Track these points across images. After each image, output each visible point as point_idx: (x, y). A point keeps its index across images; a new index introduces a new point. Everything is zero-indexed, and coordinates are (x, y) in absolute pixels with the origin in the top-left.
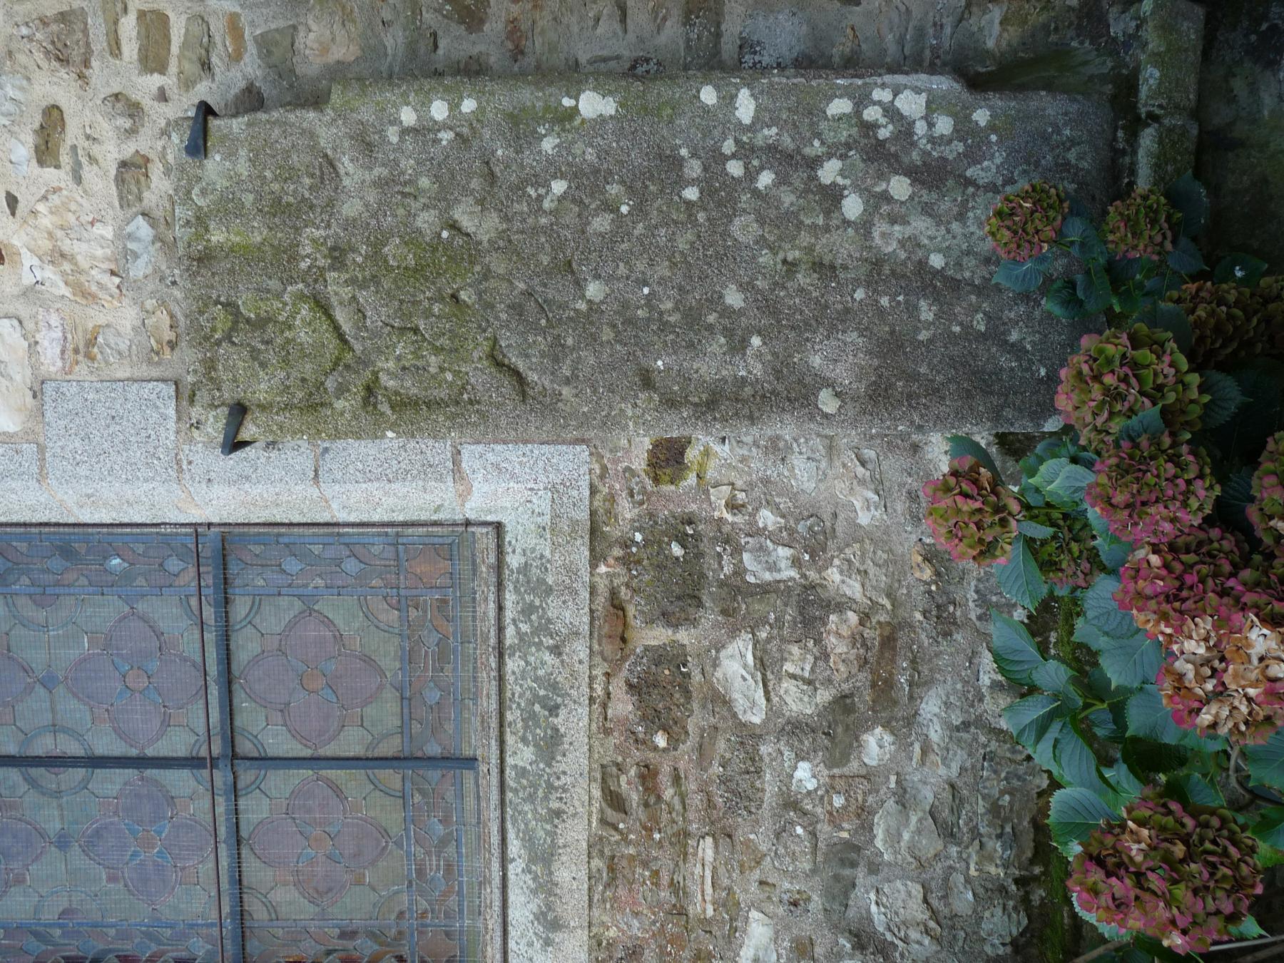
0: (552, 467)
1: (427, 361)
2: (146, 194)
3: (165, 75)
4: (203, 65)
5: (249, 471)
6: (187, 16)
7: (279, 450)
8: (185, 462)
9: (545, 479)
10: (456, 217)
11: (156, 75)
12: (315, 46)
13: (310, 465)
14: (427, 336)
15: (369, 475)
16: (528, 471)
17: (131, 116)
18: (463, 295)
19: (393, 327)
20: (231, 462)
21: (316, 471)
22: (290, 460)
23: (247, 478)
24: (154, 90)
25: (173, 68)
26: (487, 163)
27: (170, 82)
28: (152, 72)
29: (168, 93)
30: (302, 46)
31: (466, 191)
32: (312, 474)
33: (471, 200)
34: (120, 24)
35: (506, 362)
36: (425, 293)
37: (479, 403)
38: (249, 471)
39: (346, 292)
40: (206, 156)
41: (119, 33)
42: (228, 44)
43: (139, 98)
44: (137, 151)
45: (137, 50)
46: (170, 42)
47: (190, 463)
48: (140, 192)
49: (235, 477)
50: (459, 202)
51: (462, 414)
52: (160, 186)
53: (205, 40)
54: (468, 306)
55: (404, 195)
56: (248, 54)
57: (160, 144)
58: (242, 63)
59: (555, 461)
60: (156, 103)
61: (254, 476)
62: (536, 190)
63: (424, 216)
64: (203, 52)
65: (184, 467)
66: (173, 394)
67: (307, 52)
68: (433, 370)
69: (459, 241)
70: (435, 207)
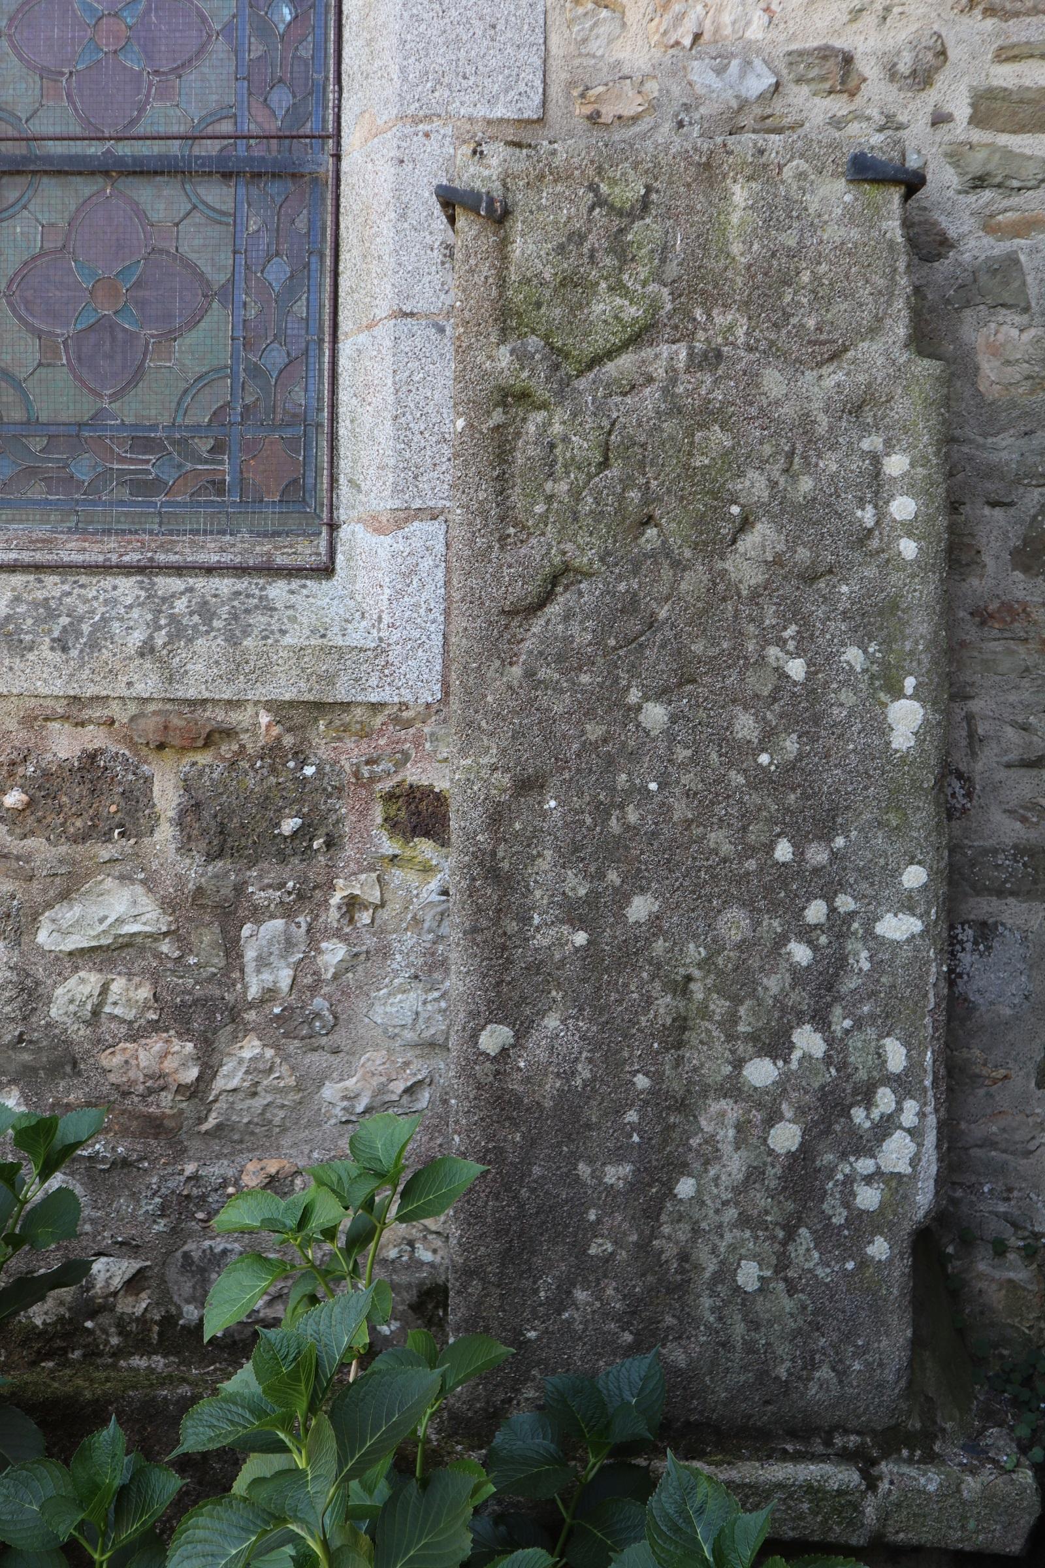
2: (805, 90)
3: (969, 123)
4: (981, 178)
5: (413, 218)
9: (395, 638)
10: (759, 526)
11: (968, 111)
13: (419, 306)
15: (404, 389)
19: (609, 433)
23: (403, 216)
24: (949, 108)
25: (978, 136)
26: (830, 572)
27: (959, 131)
28: (973, 105)
29: (945, 127)
33: (781, 547)
35: (560, 589)
36: (656, 479)
39: (659, 371)
41: (1030, 61)
42: (1009, 214)
44: (865, 80)
45: (1004, 85)
46: (1014, 132)
47: (427, 135)
48: (809, 81)
49: (405, 199)
50: (779, 532)
52: (816, 110)
53: (1015, 184)
55: (791, 455)
57: (874, 112)
58: (981, 233)
59: (420, 653)
60: (930, 109)
61: (406, 225)
62: (792, 638)
64: (998, 180)
65: (421, 126)
66: (526, 116)
67: (993, 325)
69: (726, 530)
70: (772, 497)
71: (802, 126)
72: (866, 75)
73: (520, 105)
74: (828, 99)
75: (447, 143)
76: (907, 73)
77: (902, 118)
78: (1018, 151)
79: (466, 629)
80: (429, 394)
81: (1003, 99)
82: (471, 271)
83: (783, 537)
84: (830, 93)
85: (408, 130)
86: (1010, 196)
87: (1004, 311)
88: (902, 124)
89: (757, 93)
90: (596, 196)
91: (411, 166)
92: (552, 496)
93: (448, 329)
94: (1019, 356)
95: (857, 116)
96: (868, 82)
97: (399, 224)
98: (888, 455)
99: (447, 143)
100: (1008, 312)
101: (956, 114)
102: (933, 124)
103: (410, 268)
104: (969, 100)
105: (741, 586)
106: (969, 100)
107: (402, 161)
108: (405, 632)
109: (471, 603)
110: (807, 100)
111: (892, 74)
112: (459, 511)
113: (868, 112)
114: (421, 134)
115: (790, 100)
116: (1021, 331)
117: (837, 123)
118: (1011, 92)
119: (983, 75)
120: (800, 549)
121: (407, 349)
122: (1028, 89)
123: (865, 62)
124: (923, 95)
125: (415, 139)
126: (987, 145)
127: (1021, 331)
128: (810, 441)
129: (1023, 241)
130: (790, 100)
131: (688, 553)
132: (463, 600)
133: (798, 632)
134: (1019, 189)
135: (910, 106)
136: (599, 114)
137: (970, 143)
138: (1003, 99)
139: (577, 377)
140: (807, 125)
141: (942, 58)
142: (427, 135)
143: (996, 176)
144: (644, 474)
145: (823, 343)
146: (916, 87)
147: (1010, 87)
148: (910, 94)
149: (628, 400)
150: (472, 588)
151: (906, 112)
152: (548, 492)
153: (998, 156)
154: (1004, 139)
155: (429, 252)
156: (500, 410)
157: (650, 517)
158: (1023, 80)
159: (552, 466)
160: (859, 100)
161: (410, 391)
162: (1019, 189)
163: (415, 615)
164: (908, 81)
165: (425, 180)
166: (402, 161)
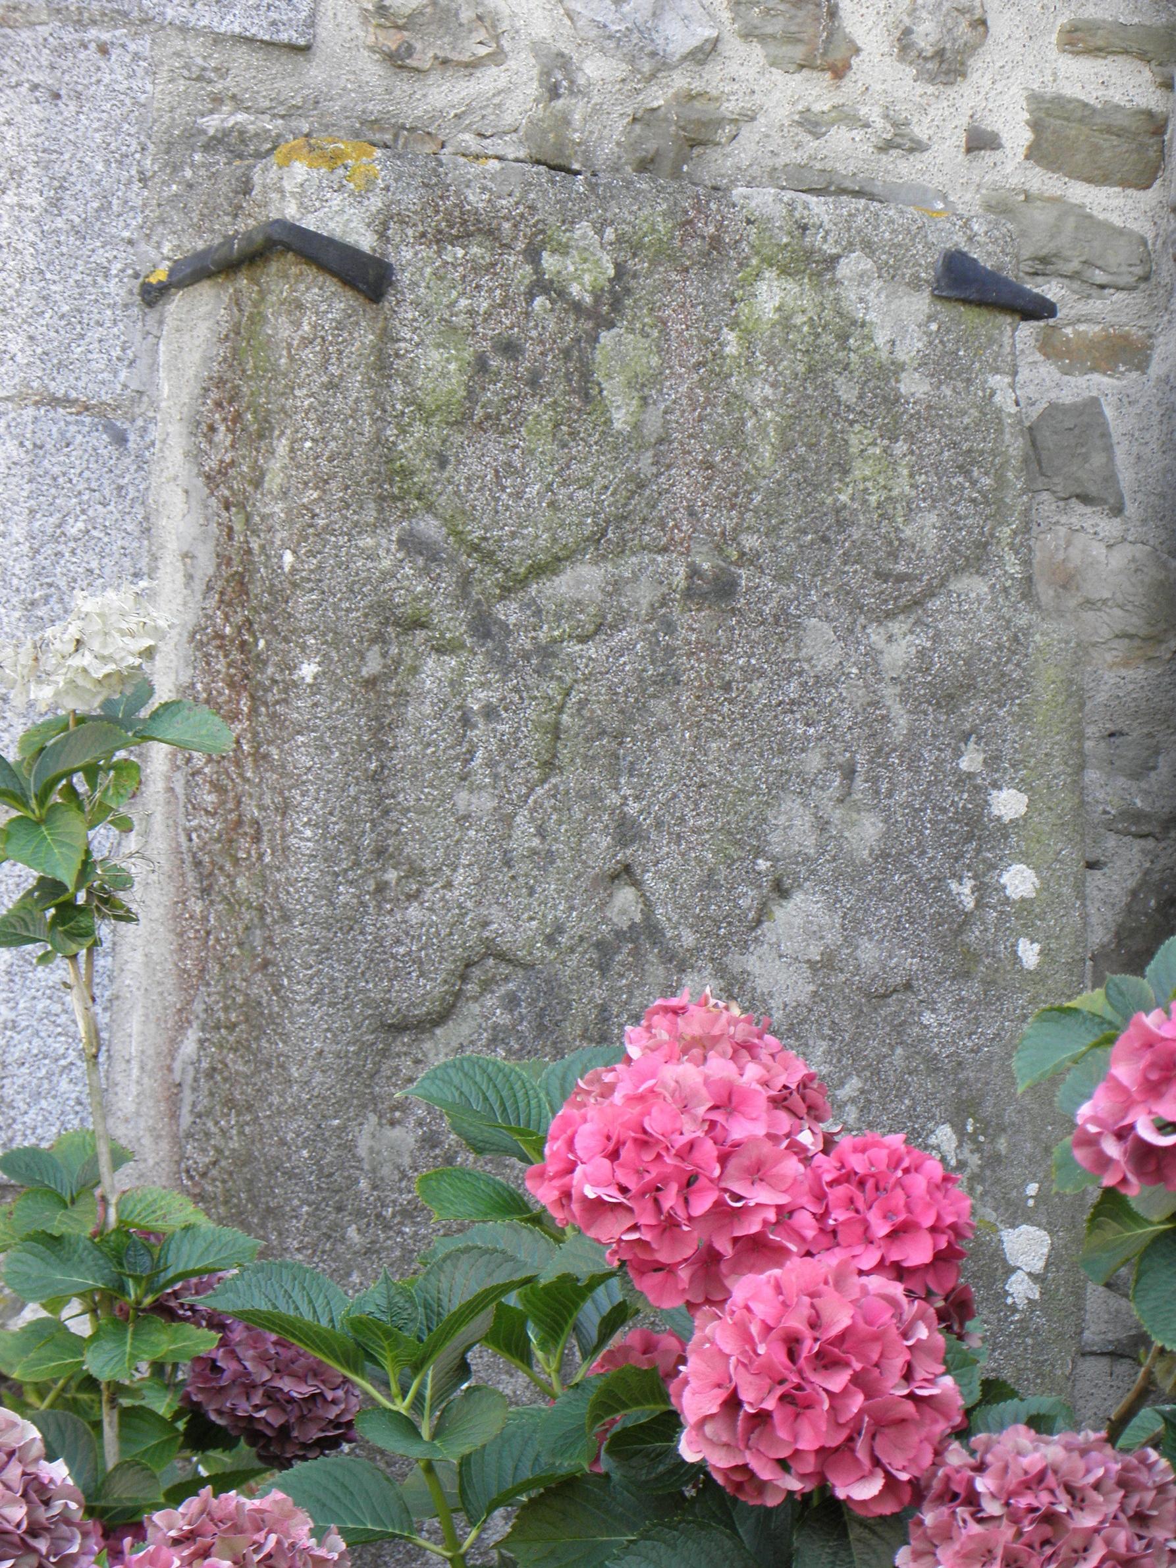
0: (49, 1076)
1: (481, 788)
2: (757, 52)
3: (1027, 157)
4: (1044, 260)
5: (74, 211)
6: (1150, 236)
7: (126, 306)
8: (106, 36)
9: (16, 1053)
10: (798, 897)
11: (1027, 136)
12: (1075, 553)
13: (80, 386)
14: (540, 791)
15: (48, 550)
16: (40, 1006)
17: (940, 54)
18: (626, 896)
19: (560, 710)
20: (100, 167)
21: (67, 401)
22: (96, 334)
23: (56, 204)
24: (993, 123)
25: (1042, 181)
26: (908, 986)
27: (1009, 168)
28: (1036, 125)
29: (988, 157)
30: (1075, 521)
31: (853, 926)
32: (58, 388)
33: (833, 938)
34: (1139, 64)
35: (471, 988)
36: (637, 798)
37: (560, 930)
38: (74, 211)
39: (644, 595)
40: (940, 298)
41: (1120, 59)
42: (1082, 328)
43: (974, 77)
44: (858, 51)
45: (1082, 97)
46: (1089, 180)
47: (104, 50)
48: (763, 39)
49: (59, 170)
50: (831, 908)
51: (356, 864)
52: (776, 95)
53: (1100, 277)
54: (604, 905)
55: (849, 773)
56: (1057, 375)
57: (873, 114)
58: (1038, 357)
59: (64, 1085)
60: (964, 121)
61: (60, 223)
62: (853, 1100)
63: (803, 822)
64: (1075, 265)
65: (93, 33)
66: (284, 37)
67: (1062, 531)
68: (462, 798)
69: (748, 898)
70: (822, 849)
71: (753, 119)
72: (860, 44)
73: (273, 15)
74: (797, 76)
75: (140, 72)
76: (930, 51)
77: (920, 131)
78: (1101, 217)
79: (321, 1053)
80: (94, 565)
81: (1081, 120)
82: (332, 386)
83: (838, 920)
84: (802, 67)
85: (69, 36)
86: (1089, 296)
87: (1080, 508)
88: (919, 142)
89: (685, 50)
90: (536, 272)
91: (73, 108)
92: (466, 817)
93: (132, 437)
94: (1106, 594)
95: (847, 117)
96: (863, 55)
97: (47, 219)
98: (996, 785)
99: (140, 72)
100: (1088, 510)
101: (1005, 138)
102: (969, 150)
103: (65, 308)
104: (1027, 116)
105: (772, 1003)
106: (1027, 116)
107: (57, 96)
108: (36, 1042)
109: (332, 1005)
110: (761, 73)
111: (904, 44)
112: (308, 833)
113: (863, 111)
114: (93, 46)
115: (733, 68)
116: (1109, 547)
117: (811, 124)
118: (1094, 110)
119: (1048, 72)
120: (865, 943)
121: (56, 470)
122: (1118, 107)
123: (857, 17)
124: (950, 91)
125: (82, 55)
126: (1054, 200)
127: (1109, 547)
128: (879, 750)
129: (1106, 380)
130: (733, 68)
131: (689, 939)
132: (316, 1000)
133: (862, 1092)
134: (1102, 287)
135: (932, 112)
136: (410, 50)
137: (1025, 192)
138: (1081, 120)
139: (502, 598)
140: (762, 120)
141: (981, 29)
142: (104, 50)
143: (1067, 260)
144: (616, 789)
145: (901, 578)
146: (943, 78)
147: (1092, 102)
148: (931, 89)
149: (591, 649)
150: (332, 979)
151: (926, 120)
152: (462, 810)
153: (1071, 223)
154: (1080, 193)
155: (100, 280)
156: (376, 648)
157: (627, 869)
158: (1111, 92)
159: (467, 762)
160: (850, 87)
161: (59, 554)
162: (1102, 287)
163: (57, 1008)
164: (930, 66)
165: (98, 137)
166: (57, 96)
